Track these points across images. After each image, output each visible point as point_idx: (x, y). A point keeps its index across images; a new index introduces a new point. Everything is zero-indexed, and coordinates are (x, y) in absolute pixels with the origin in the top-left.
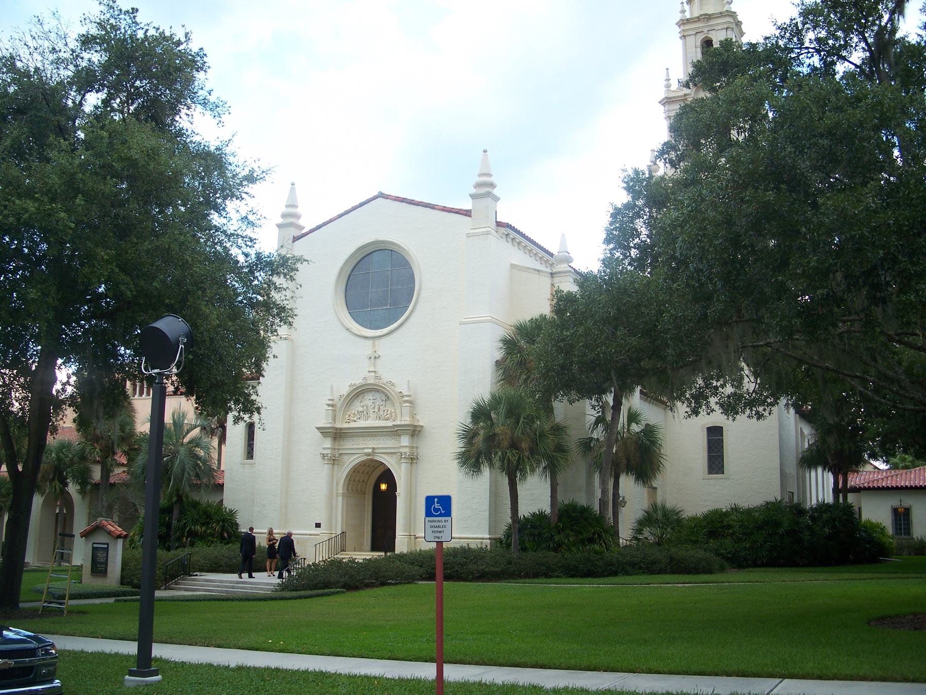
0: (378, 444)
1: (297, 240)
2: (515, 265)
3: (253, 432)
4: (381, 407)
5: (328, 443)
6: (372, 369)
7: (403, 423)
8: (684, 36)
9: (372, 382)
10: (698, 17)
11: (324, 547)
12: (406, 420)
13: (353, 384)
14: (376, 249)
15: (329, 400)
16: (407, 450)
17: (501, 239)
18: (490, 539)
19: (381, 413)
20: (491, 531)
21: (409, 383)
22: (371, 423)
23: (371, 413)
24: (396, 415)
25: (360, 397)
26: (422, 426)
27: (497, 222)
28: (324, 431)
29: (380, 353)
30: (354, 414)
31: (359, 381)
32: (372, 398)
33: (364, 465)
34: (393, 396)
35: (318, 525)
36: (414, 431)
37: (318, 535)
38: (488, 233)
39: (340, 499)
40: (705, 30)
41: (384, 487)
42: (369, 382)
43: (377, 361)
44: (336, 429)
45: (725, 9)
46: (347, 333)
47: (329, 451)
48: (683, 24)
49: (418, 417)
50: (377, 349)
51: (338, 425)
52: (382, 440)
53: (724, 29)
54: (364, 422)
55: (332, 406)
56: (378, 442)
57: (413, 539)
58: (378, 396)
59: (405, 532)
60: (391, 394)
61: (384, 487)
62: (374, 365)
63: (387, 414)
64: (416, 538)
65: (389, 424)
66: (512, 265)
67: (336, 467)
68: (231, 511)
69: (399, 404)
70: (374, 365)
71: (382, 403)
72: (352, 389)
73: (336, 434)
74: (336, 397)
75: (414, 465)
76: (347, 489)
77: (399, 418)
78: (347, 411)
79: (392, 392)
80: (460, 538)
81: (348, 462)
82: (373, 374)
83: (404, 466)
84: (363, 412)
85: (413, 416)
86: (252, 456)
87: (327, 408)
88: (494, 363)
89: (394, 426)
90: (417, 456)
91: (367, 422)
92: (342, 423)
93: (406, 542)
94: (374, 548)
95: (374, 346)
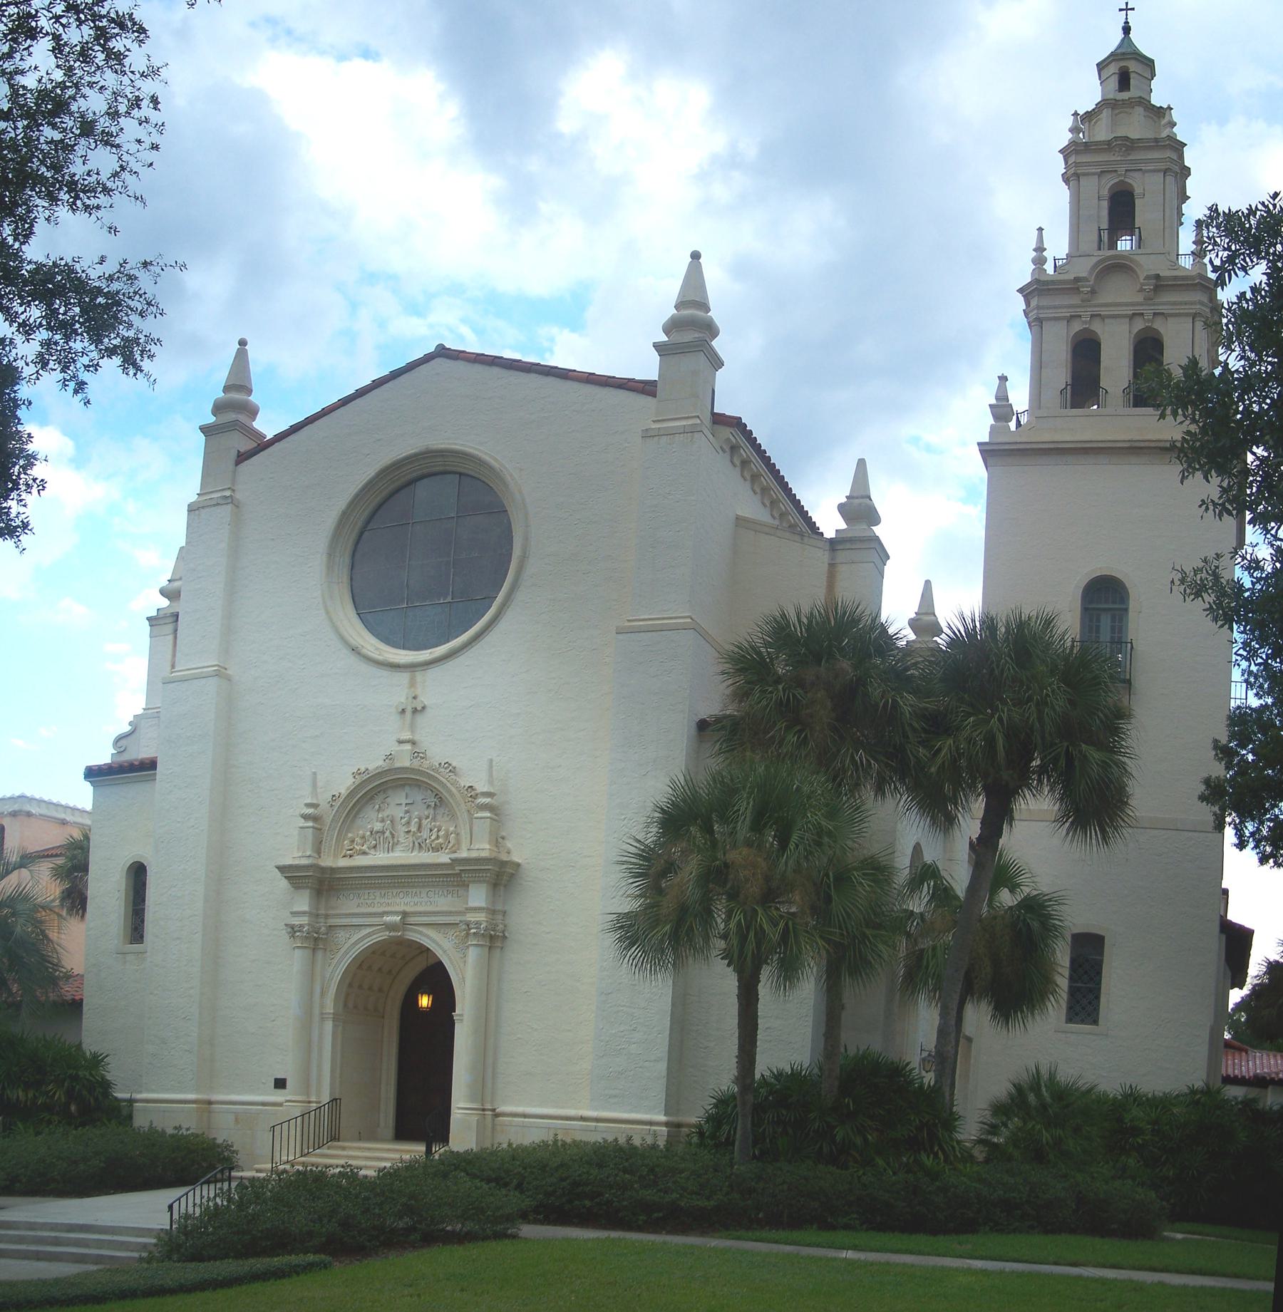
0: (416, 904)
1: (246, 459)
2: (745, 520)
3: (144, 884)
4: (424, 822)
5: (303, 903)
6: (406, 735)
7: (474, 854)
8: (1077, 176)
9: (407, 764)
10: (1109, 143)
11: (292, 1132)
12: (482, 848)
13: (363, 769)
14: (425, 471)
15: (308, 805)
16: (481, 917)
17: (720, 451)
18: (667, 1124)
19: (425, 834)
20: (673, 1101)
21: (491, 766)
22: (401, 856)
23: (402, 834)
24: (458, 842)
25: (378, 800)
26: (518, 865)
27: (714, 414)
28: (292, 874)
29: (424, 699)
30: (363, 837)
31: (374, 762)
32: (404, 801)
33: (383, 954)
34: (452, 795)
35: (280, 1084)
36: (499, 875)
37: (280, 1105)
38: (693, 430)
39: (329, 1026)
40: (1122, 169)
41: (425, 1001)
42: (398, 765)
43: (419, 718)
44: (323, 870)
45: (1164, 135)
46: (352, 659)
47: (304, 920)
48: (1077, 152)
49: (509, 844)
50: (419, 691)
51: (327, 861)
52: (424, 895)
53: (1159, 171)
54: (386, 855)
55: (315, 818)
56: (416, 899)
57: (489, 1119)
58: (418, 796)
59: (472, 1101)
60: (449, 791)
61: (425, 1001)
62: (412, 728)
63: (438, 837)
64: (497, 1115)
65: (444, 858)
66: (738, 518)
67: (320, 954)
68: (95, 1056)
69: (466, 814)
70: (412, 728)
71: (426, 813)
72: (359, 779)
73: (321, 882)
74: (324, 798)
75: (497, 953)
76: (345, 1005)
77: (464, 845)
78: (348, 831)
79: (453, 789)
80: (597, 1120)
81: (346, 946)
82: (408, 747)
83: (472, 954)
84: (383, 833)
85: (498, 840)
86: (142, 937)
87: (302, 823)
88: (694, 725)
89: (455, 861)
90: (503, 932)
91: (391, 854)
92: (335, 856)
93: (474, 1124)
94: (403, 1133)
95: (412, 684)
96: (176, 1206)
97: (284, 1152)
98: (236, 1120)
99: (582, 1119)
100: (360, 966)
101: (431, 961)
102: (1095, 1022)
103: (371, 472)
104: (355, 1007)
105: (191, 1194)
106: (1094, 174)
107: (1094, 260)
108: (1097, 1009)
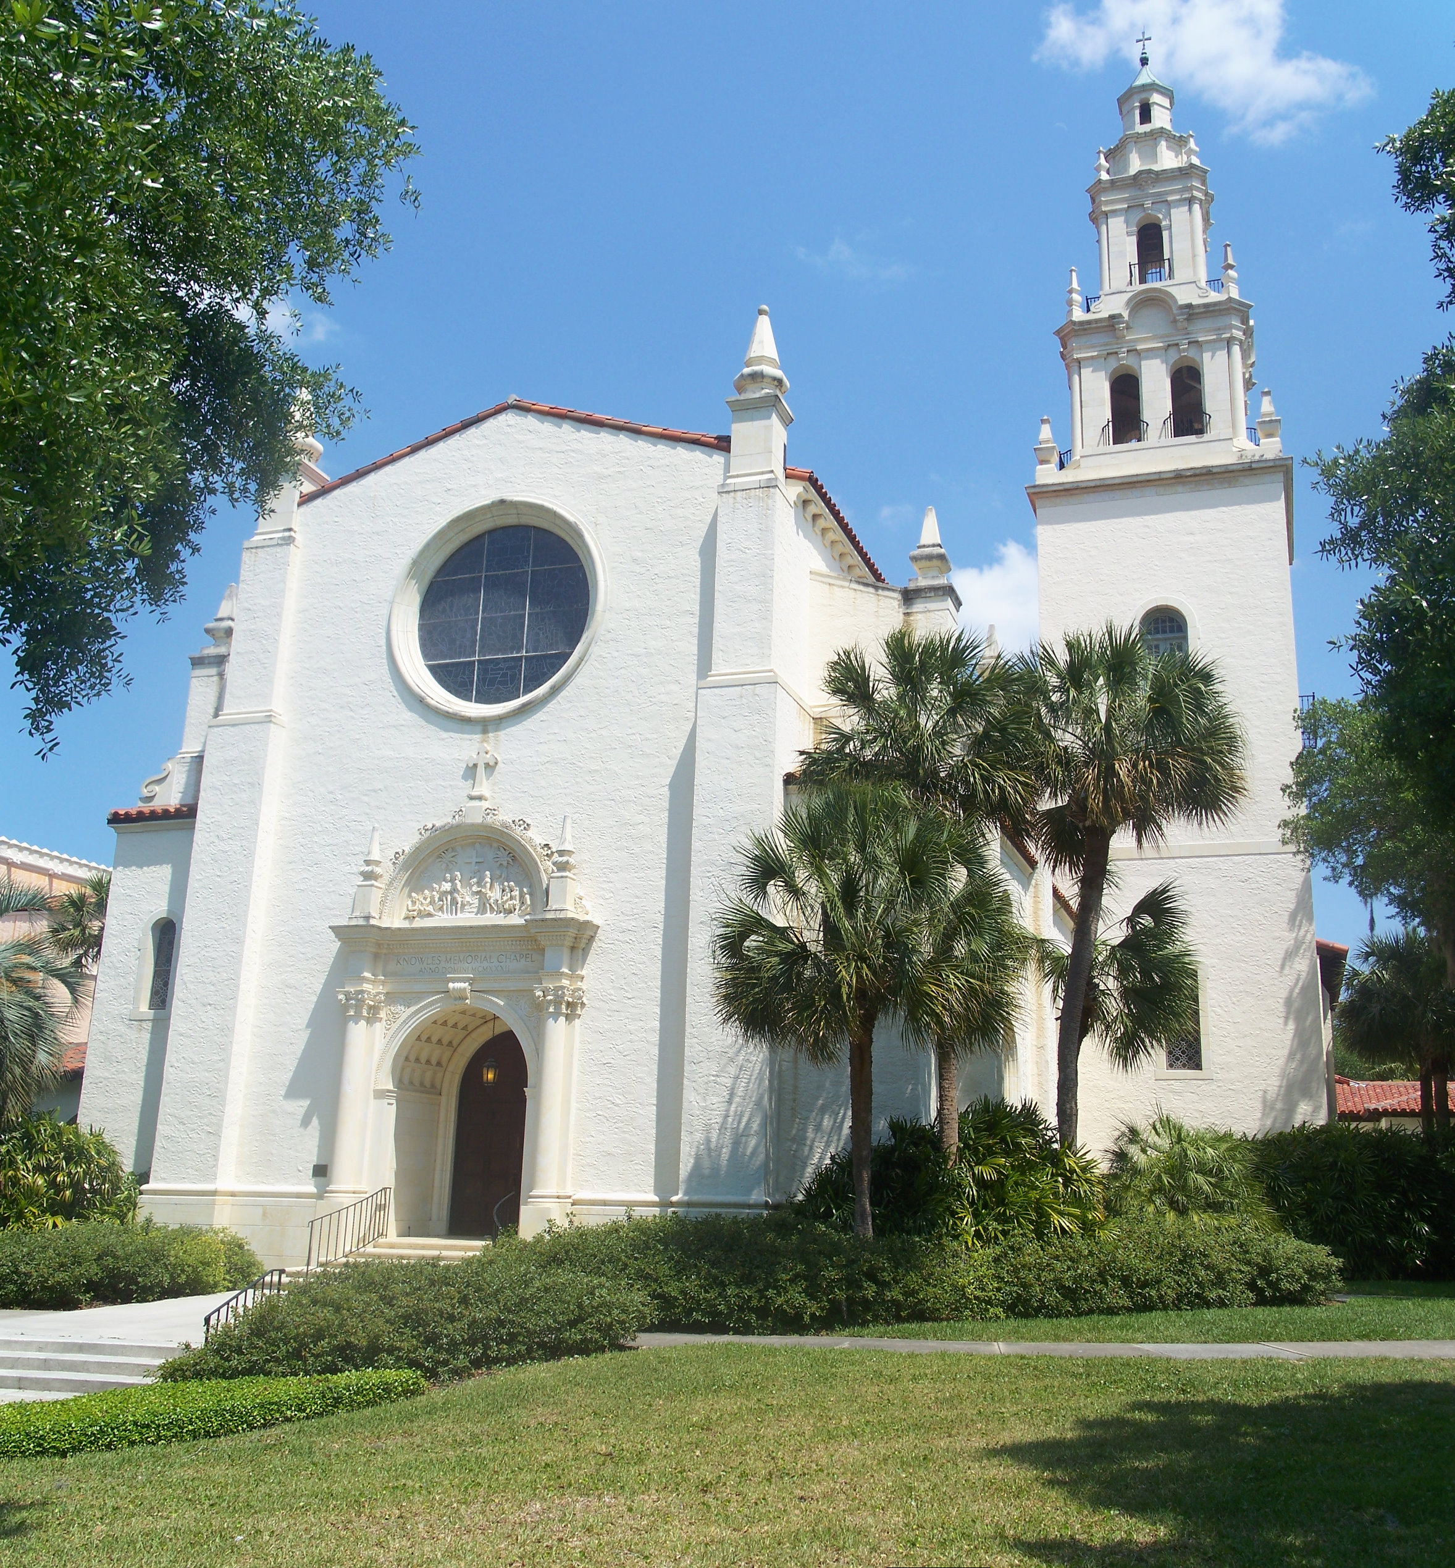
13: (430, 826)
33: (445, 1023)
73: (912, 1166)
94: (458, 1227)
96: (214, 1317)
97: (323, 1251)
98: (264, 1214)
99: (605, 1203)
100: (419, 1038)
101: (498, 1030)
102: (1198, 1066)
103: (442, 522)
104: (411, 1083)
105: (242, 1297)
106: (1121, 210)
107: (1126, 297)
108: (1198, 1052)
